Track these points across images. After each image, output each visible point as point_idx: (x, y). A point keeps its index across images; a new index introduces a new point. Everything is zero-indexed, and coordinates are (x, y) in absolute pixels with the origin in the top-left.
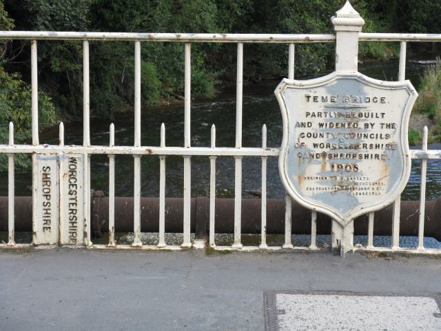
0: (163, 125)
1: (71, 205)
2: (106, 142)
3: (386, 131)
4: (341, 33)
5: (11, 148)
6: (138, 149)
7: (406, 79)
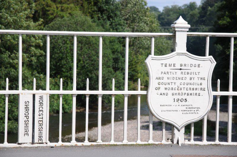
0: (219, 80)
1: (40, 121)
2: (84, 88)
3: (200, 81)
4: (180, 33)
5: (7, 92)
6: (126, 92)
7: (209, 55)
